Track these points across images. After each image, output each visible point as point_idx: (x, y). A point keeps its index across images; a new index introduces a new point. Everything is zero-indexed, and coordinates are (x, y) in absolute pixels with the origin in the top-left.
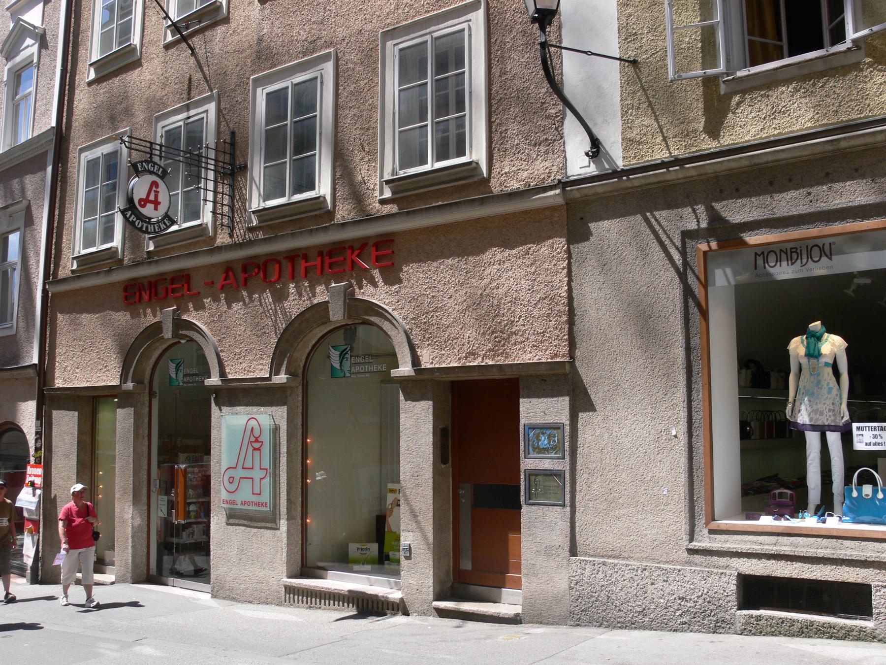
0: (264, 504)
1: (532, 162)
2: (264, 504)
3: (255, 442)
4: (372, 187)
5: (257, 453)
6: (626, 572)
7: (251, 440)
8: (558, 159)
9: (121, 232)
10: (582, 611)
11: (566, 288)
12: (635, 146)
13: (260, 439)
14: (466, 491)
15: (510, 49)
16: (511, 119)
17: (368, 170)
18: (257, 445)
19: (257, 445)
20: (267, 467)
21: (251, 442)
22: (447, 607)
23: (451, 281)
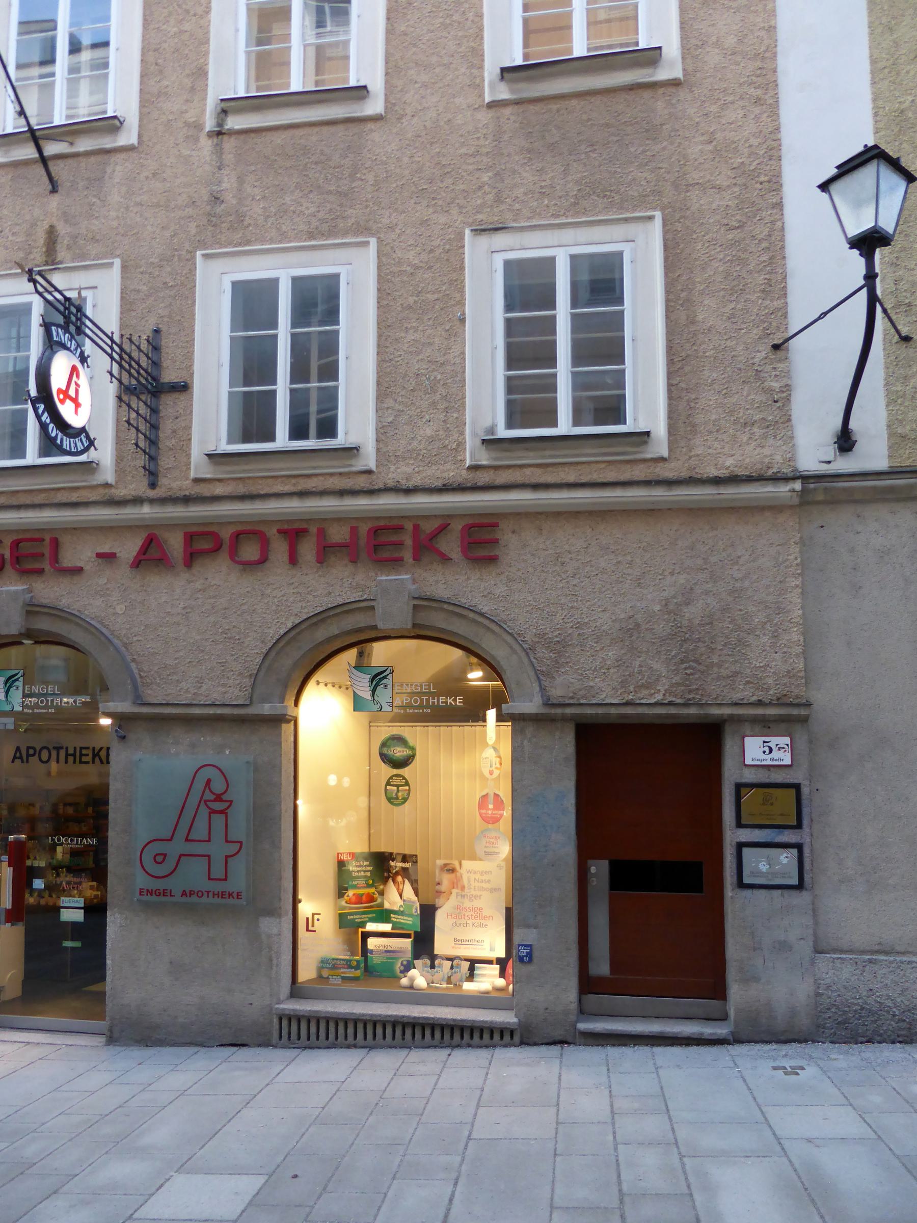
0: (235, 895)
1: (740, 446)
2: (235, 895)
3: (215, 800)
4: (454, 446)
5: (218, 820)
6: (908, 971)
7: (205, 798)
8: (784, 447)
9: (319, 118)
10: (837, 1024)
11: (800, 612)
12: (910, 445)
13: (224, 797)
14: (599, 869)
15: (702, 293)
16: (706, 385)
17: (444, 421)
18: (218, 806)
19: (218, 806)
20: (243, 838)
21: (205, 801)
22: (607, 1030)
23: (604, 589)
